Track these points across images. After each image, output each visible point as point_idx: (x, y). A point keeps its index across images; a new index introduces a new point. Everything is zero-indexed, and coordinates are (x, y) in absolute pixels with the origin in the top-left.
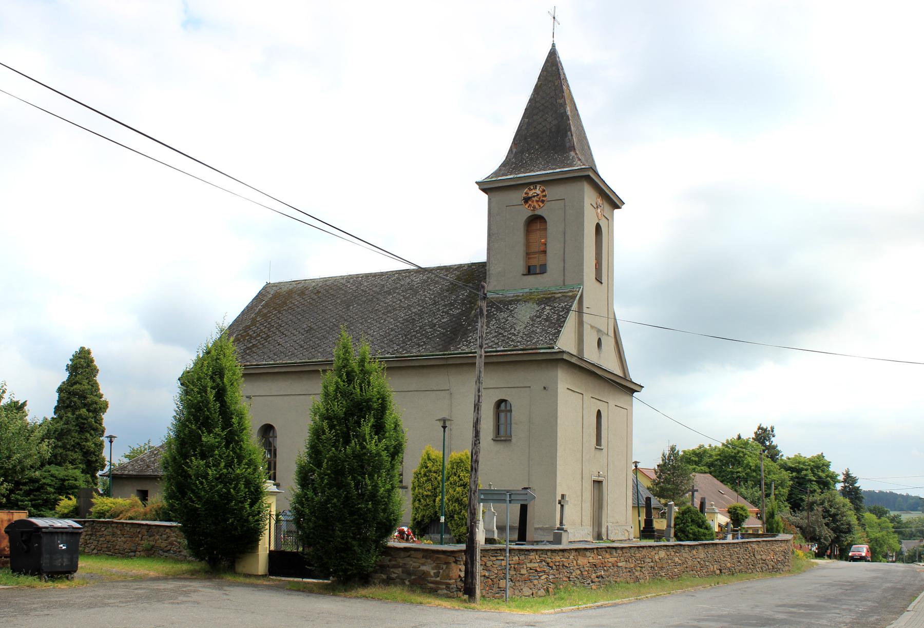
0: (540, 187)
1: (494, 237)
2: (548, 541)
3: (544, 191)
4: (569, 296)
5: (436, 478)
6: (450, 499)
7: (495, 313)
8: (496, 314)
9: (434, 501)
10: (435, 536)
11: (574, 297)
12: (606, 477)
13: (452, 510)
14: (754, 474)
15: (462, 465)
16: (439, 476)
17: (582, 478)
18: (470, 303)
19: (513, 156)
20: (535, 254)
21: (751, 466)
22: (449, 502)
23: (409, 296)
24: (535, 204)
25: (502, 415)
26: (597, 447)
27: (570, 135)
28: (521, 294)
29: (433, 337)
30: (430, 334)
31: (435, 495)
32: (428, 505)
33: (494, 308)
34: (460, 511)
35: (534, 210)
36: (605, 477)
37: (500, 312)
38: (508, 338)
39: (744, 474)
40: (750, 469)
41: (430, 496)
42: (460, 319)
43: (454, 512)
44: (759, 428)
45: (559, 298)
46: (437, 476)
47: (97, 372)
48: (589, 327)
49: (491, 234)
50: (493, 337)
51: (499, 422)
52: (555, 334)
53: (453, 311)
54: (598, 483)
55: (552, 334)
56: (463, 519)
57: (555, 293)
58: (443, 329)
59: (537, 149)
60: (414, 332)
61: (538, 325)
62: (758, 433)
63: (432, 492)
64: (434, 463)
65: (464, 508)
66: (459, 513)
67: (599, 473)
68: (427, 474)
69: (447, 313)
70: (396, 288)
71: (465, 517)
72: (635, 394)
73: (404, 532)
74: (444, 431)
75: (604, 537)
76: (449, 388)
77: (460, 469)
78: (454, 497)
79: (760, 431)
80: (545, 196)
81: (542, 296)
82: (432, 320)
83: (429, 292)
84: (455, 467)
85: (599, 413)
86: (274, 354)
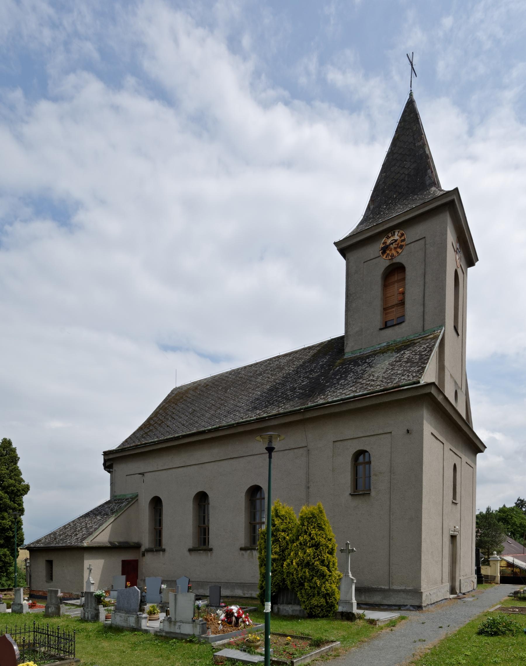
0: (399, 232)
1: (352, 297)
2: (411, 606)
3: (402, 235)
4: (430, 339)
5: (285, 538)
6: (300, 563)
7: (353, 368)
8: (354, 369)
9: (282, 566)
10: (285, 608)
11: (436, 338)
12: (459, 532)
13: (301, 577)
14: (519, 529)
15: (314, 520)
16: (288, 535)
17: (442, 533)
18: (329, 365)
19: (370, 212)
20: (392, 308)
21: (517, 524)
22: (298, 567)
23: (276, 373)
24: (394, 252)
25: (361, 468)
26: (454, 501)
27: (430, 172)
28: (379, 349)
29: (292, 398)
30: (290, 396)
31: (283, 558)
32: (276, 570)
33: (352, 365)
34: (311, 577)
35: (392, 259)
36: (458, 532)
37: (358, 366)
38: (367, 384)
39: (512, 530)
40: (517, 526)
41: (278, 559)
42: (319, 379)
43: (304, 578)
44: (518, 500)
45: (419, 342)
46: (285, 536)
47: (18, 460)
49: (349, 295)
50: (351, 387)
51: (357, 476)
52: (418, 371)
53: (313, 375)
54: (453, 538)
55: (415, 372)
56: (314, 588)
57: (414, 340)
58: (303, 390)
59: (396, 198)
60: (276, 397)
61: (399, 367)
62: (517, 503)
63: (280, 555)
64: (283, 520)
65: (316, 574)
66: (310, 581)
67: (455, 527)
68: (275, 534)
69: (308, 377)
70: (267, 370)
71: (317, 586)
73: (233, 613)
75: (458, 591)
76: (306, 445)
77: (312, 525)
78: (304, 561)
79: (519, 501)
80: (403, 240)
81: (401, 345)
82: (293, 385)
83: (293, 366)
84: (306, 523)
85: (455, 466)
86: (162, 434)
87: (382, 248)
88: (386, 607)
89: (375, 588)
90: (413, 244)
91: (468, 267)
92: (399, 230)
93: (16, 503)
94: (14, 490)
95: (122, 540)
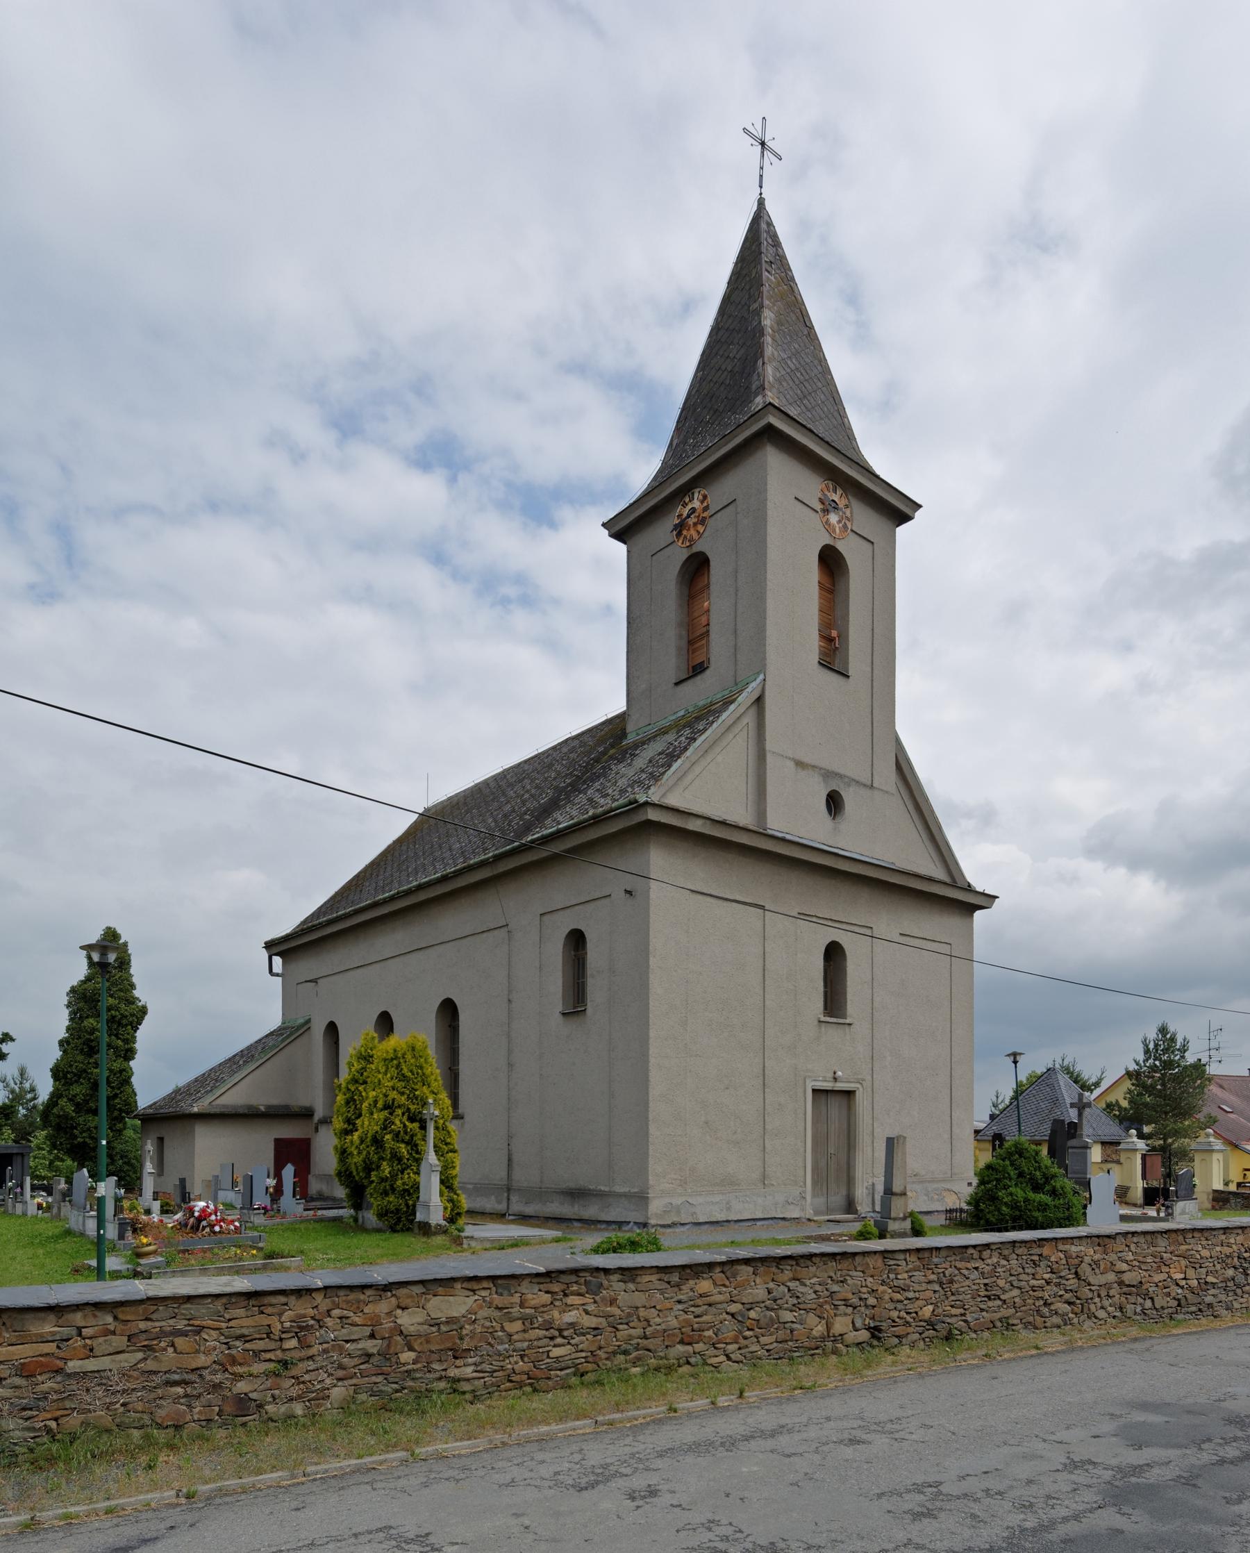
3: (705, 497)
35: (691, 546)
48: (791, 764)
67: (835, 1073)
72: (978, 915)
74: (1016, 1067)
80: (706, 509)
87: (676, 527)
88: (603, 1226)
89: (594, 1190)
90: (719, 514)
91: (898, 526)
92: (698, 489)
93: (120, 1039)
94: (115, 1016)
95: (275, 1101)
